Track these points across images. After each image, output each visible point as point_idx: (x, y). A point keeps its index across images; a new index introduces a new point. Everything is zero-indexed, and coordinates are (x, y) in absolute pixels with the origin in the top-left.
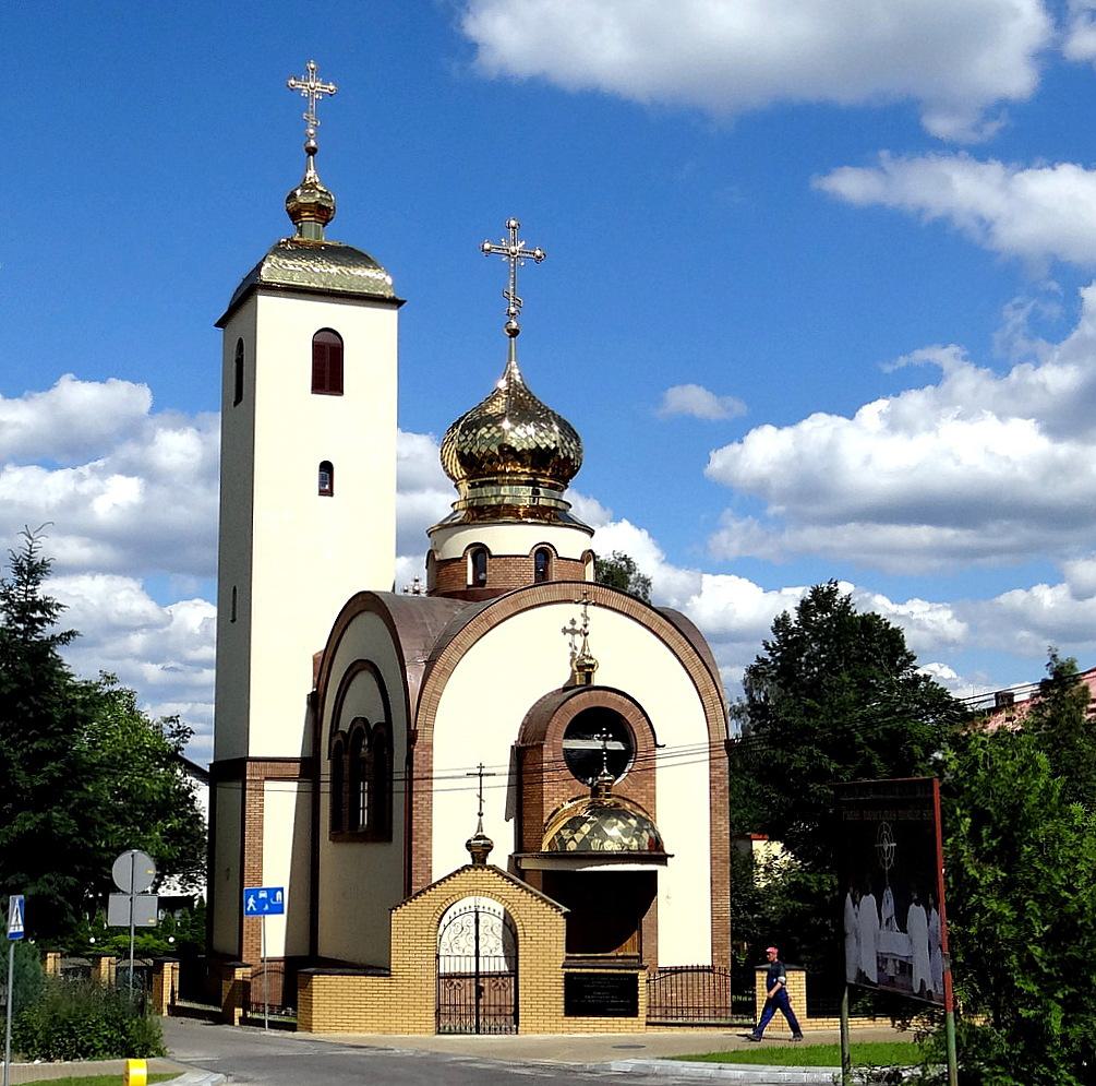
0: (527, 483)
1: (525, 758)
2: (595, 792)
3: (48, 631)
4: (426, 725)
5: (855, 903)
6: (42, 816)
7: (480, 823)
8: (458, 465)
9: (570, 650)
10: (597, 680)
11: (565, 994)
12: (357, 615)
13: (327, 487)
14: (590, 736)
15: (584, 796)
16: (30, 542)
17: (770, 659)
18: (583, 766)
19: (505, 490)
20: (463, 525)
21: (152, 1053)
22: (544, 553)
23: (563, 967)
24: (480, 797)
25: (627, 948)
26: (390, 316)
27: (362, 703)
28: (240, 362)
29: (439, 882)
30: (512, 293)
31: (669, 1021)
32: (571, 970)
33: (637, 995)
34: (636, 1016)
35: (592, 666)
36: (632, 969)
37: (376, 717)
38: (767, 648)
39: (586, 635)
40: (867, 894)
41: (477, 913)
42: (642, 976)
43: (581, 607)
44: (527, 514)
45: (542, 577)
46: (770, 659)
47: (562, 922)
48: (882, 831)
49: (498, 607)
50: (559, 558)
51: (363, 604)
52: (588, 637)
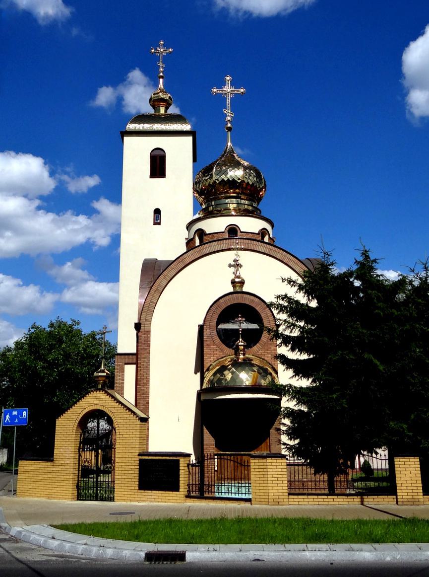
4: (146, 320)
11: (139, 474)
23: (139, 455)
33: (422, 483)
34: (178, 491)
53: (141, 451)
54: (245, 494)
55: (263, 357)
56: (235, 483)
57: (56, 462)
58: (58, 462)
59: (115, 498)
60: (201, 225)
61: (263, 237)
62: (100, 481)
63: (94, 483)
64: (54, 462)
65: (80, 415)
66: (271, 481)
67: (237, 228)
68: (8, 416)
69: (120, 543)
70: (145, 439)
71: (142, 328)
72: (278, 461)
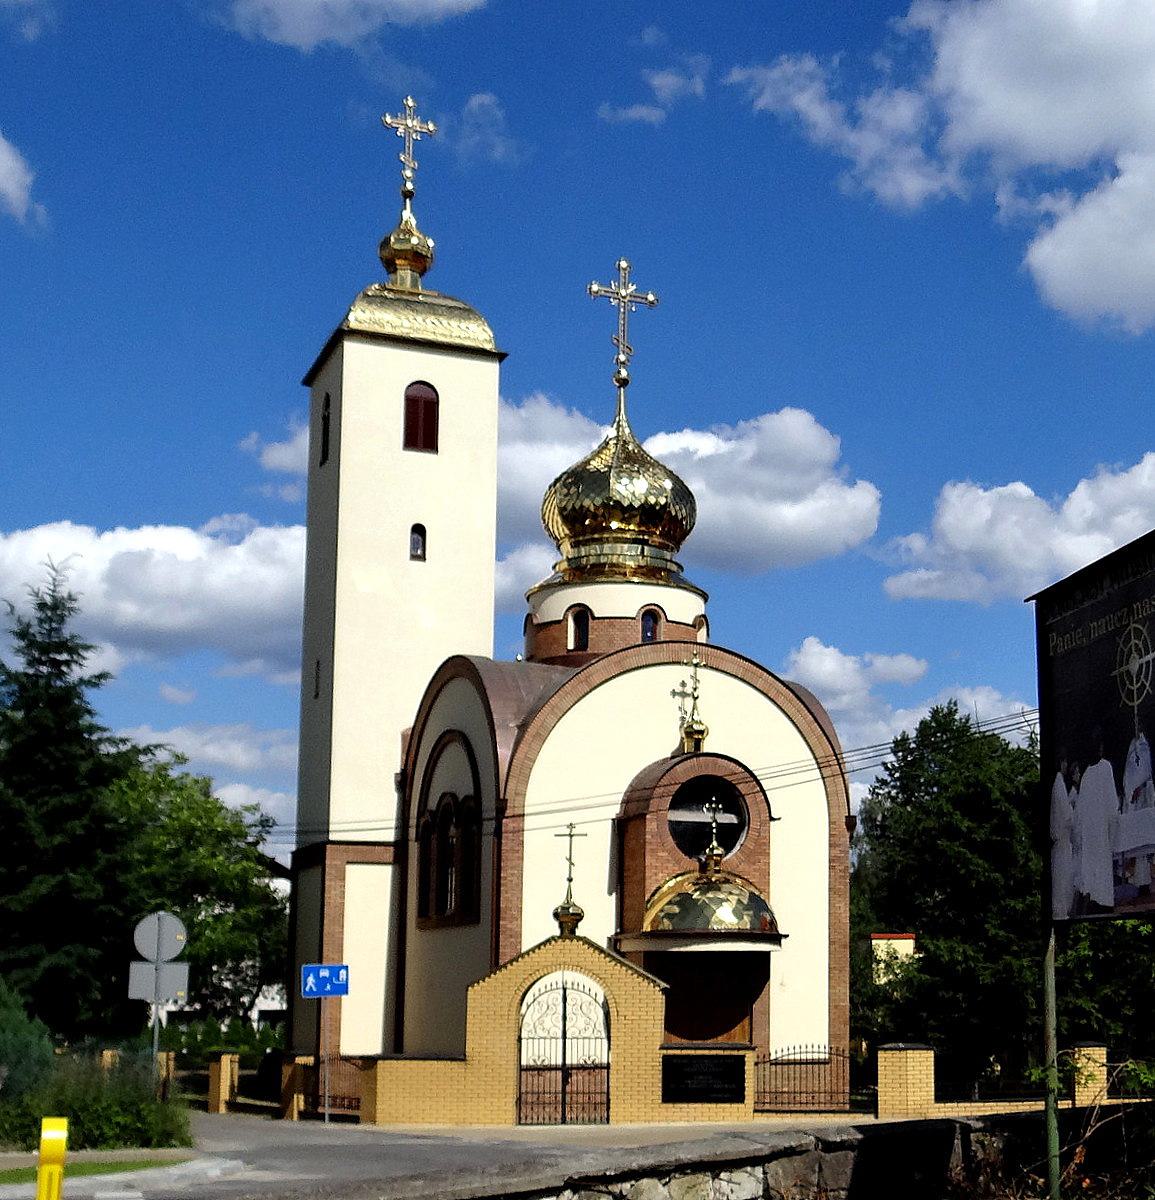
0: (635, 541)
1: (627, 829)
2: (703, 868)
3: (75, 673)
5: (1071, 783)
6: (59, 878)
7: (570, 886)
8: (560, 522)
9: (679, 714)
10: (707, 746)
12: (446, 683)
13: (419, 552)
14: (699, 806)
15: (689, 872)
16: (54, 573)
17: (889, 779)
18: (691, 839)
19: (607, 548)
20: (564, 584)
21: (174, 1142)
22: (651, 616)
23: (661, 1048)
24: (570, 859)
25: (738, 1034)
26: (492, 369)
27: (452, 776)
28: (326, 419)
29: (527, 953)
30: (621, 340)
31: (779, 1107)
32: (671, 1052)
35: (701, 732)
36: (739, 1049)
37: (465, 788)
38: (887, 769)
39: (696, 698)
40: (1095, 761)
41: (565, 990)
42: (750, 1058)
43: (691, 669)
44: (634, 574)
45: (650, 638)
46: (889, 779)
47: (660, 999)
48: (1128, 640)
49: (597, 669)
50: (668, 621)
51: (457, 669)
52: (697, 701)
67: (660, 611)
68: (311, 980)
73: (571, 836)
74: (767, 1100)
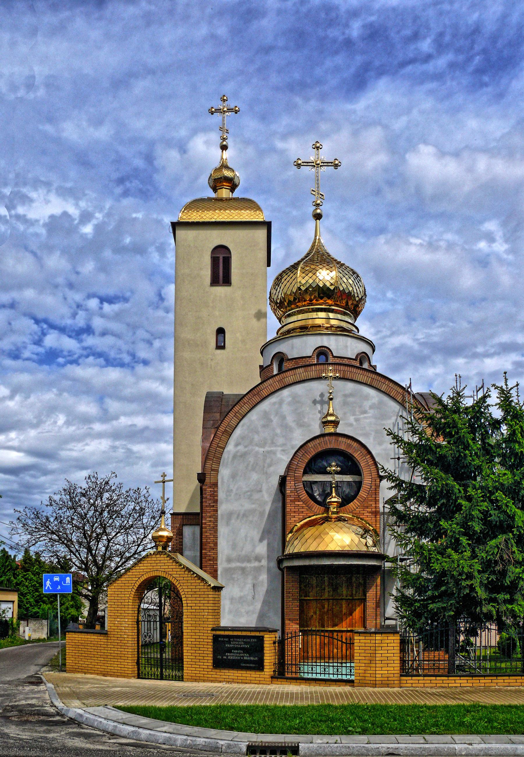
23: (212, 630)
53: (214, 626)
54: (333, 674)
55: (361, 517)
56: (320, 663)
57: (111, 636)
58: (113, 636)
59: (184, 677)
60: (284, 347)
61: (361, 364)
62: (166, 659)
63: (157, 661)
64: (109, 636)
65: (137, 582)
66: (376, 661)
68: (48, 583)
69: (212, 732)
70: (217, 613)
71: (207, 480)
72: (389, 638)
73: (164, 482)
74: (318, 671)
